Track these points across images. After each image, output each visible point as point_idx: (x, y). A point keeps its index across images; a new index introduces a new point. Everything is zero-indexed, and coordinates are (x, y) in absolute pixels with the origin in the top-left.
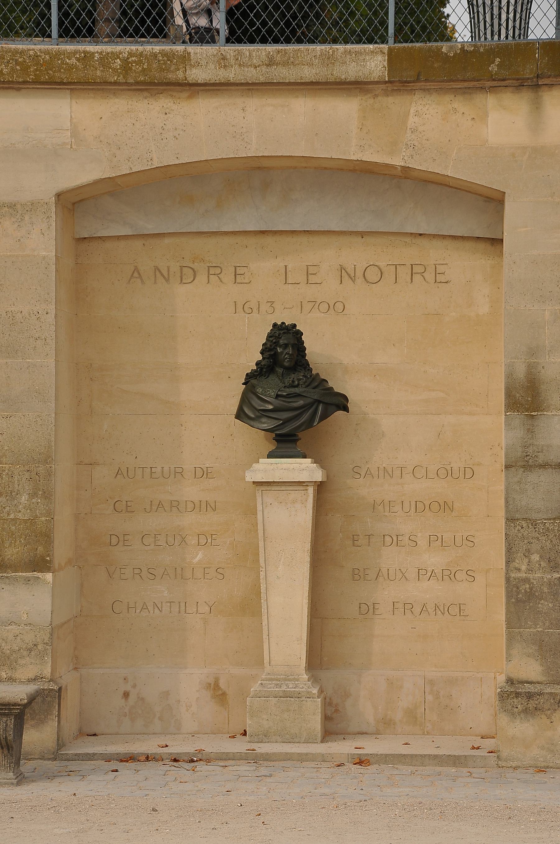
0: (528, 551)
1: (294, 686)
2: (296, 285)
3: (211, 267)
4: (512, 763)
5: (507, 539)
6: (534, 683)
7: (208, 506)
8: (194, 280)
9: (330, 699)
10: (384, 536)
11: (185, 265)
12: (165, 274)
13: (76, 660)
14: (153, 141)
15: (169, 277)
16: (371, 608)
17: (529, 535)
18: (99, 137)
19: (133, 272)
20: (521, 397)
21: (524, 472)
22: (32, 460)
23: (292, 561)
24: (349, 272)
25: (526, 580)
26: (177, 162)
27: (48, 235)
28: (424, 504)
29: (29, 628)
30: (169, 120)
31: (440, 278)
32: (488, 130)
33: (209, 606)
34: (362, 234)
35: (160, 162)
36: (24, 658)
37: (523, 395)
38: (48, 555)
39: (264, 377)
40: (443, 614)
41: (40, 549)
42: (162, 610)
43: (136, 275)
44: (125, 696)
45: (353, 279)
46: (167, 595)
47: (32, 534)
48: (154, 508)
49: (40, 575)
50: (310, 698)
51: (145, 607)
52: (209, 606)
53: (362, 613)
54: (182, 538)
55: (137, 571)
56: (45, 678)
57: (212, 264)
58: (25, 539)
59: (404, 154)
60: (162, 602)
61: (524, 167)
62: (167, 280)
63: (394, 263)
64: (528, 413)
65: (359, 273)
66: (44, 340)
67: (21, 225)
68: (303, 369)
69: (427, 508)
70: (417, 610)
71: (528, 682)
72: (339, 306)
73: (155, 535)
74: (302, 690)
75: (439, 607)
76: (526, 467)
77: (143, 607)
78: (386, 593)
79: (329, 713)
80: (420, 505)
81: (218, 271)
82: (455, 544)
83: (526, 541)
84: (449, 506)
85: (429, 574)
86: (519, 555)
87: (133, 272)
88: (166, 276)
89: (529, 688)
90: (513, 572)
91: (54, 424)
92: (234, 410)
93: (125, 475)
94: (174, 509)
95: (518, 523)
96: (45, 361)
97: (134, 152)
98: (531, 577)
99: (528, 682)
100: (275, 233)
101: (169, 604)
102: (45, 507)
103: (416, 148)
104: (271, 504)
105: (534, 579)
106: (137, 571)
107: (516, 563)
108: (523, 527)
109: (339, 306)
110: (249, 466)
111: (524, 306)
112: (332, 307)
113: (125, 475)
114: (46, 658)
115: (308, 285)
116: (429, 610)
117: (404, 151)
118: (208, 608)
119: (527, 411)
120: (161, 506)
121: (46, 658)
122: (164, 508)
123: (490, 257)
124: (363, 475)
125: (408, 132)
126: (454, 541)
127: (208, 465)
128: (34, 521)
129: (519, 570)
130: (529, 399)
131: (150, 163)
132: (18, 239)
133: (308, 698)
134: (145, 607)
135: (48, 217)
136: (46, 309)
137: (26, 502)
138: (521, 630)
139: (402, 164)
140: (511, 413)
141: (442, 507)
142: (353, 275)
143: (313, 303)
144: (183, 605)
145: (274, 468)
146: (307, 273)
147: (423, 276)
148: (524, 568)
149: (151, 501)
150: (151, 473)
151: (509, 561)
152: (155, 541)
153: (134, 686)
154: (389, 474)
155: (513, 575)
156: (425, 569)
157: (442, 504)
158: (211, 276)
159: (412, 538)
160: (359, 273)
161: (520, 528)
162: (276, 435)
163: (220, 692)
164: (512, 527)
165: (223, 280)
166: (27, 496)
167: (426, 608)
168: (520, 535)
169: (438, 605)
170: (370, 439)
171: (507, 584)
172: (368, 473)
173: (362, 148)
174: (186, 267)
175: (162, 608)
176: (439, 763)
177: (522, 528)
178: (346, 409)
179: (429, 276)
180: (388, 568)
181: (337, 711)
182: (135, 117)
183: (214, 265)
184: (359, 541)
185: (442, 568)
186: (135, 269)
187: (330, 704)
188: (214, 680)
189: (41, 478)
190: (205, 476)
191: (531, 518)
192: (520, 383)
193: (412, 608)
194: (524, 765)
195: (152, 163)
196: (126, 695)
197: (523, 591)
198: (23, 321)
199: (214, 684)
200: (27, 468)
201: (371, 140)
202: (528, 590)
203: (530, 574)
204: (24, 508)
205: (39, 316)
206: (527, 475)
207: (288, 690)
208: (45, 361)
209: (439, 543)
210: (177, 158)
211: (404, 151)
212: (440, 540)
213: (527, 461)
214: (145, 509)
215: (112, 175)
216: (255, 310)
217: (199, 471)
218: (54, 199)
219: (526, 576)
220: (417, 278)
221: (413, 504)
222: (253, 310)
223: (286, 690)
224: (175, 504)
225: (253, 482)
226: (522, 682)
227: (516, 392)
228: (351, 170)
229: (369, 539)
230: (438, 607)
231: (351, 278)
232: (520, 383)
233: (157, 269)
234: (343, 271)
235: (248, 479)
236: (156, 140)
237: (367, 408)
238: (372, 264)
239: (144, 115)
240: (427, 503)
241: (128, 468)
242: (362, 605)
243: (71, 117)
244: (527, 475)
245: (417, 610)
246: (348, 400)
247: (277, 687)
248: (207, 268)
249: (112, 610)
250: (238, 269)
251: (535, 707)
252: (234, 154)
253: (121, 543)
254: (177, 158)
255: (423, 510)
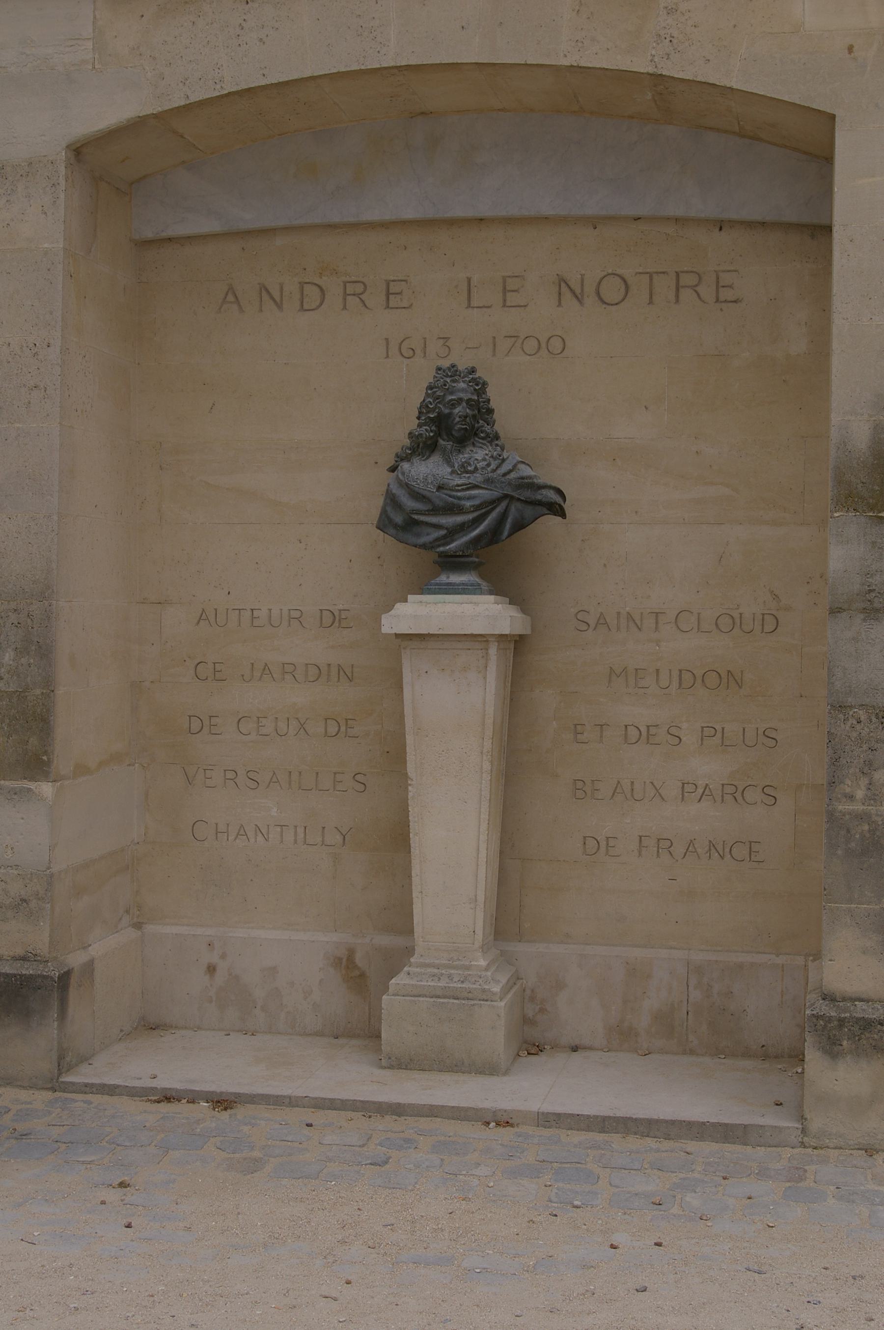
0: (869, 764)
1: (462, 979)
2: (485, 309)
3: (350, 282)
4: (828, 1141)
5: (830, 741)
6: (872, 1001)
7: (342, 672)
8: (321, 304)
9: (533, 991)
10: (626, 726)
11: (308, 281)
12: (276, 295)
13: (139, 910)
14: (224, 49)
15: (282, 303)
16: (603, 844)
17: (872, 734)
18: (138, 47)
19: (227, 294)
20: (862, 484)
21: (864, 620)
22: (21, 592)
23: (461, 770)
24: (572, 287)
25: (862, 817)
26: (263, 82)
27: (53, 214)
28: (693, 674)
29: (16, 872)
30: (252, 12)
31: (725, 294)
32: (804, 5)
33: (342, 834)
34: (594, 222)
35: (235, 83)
36: (8, 922)
37: (864, 481)
38: (45, 753)
39: (423, 457)
40: (722, 858)
41: (34, 741)
42: (268, 838)
43: (231, 298)
44: (209, 971)
45: (580, 300)
46: (275, 814)
47: (20, 717)
48: (257, 674)
49: (32, 785)
50: (487, 1000)
51: (242, 832)
52: (342, 834)
53: (587, 853)
54: (301, 724)
55: (230, 775)
56: (40, 956)
57: (350, 277)
58: (9, 725)
59: (653, 52)
60: (268, 826)
61: (869, 68)
62: (279, 306)
63: (648, 270)
64: (874, 513)
65: (590, 289)
66: (43, 391)
67: (12, 200)
68: (488, 444)
69: (699, 681)
70: (679, 849)
71: (861, 1000)
72: (556, 344)
73: (258, 718)
74: (474, 986)
75: (716, 846)
76: (868, 611)
77: (238, 833)
78: (629, 821)
79: (530, 1013)
80: (686, 676)
81: (359, 288)
82: (744, 741)
83: (865, 747)
84: (736, 678)
85: (700, 791)
86: (851, 771)
87: (227, 294)
88: (278, 299)
89: (864, 1010)
90: (840, 802)
91: (57, 533)
92: (375, 514)
93: (212, 620)
94: (288, 677)
95: (851, 713)
96: (43, 425)
97: (192, 69)
98: (872, 811)
99: (861, 1000)
100: (452, 223)
101: (279, 829)
102: (40, 671)
103: (675, 41)
104: (427, 672)
105: (877, 815)
106: (230, 775)
107: (846, 786)
108: (861, 721)
109: (556, 344)
110: (389, 608)
111: (869, 318)
112: (544, 345)
113: (212, 620)
114: (42, 924)
115: (506, 309)
116: (699, 850)
117: (654, 48)
118: (339, 838)
119: (872, 509)
120: (267, 672)
121: (42, 924)
122: (272, 675)
123: (809, 258)
124: (592, 625)
125: (661, 13)
126: (742, 737)
127: (341, 607)
128: (23, 695)
129: (851, 798)
130: (877, 488)
131: (218, 87)
132: (7, 223)
133: (483, 1000)
134: (242, 832)
135: (53, 184)
136: (47, 339)
137: (11, 663)
138: (852, 906)
139: (651, 70)
140: (842, 514)
141: (725, 680)
142: (578, 291)
143: (513, 339)
144: (300, 831)
145: (430, 611)
146: (505, 288)
147: (696, 291)
148: (860, 794)
149: (252, 664)
150: (253, 618)
151: (834, 782)
152: (258, 728)
153: (223, 956)
154: (636, 624)
155: (840, 807)
156: (694, 782)
157: (724, 675)
158: (349, 298)
159: (673, 731)
160: (590, 289)
161: (855, 722)
162: (441, 555)
163: (357, 973)
164: (840, 720)
165: (367, 303)
166: (12, 653)
167: (694, 847)
168: (855, 734)
169: (714, 843)
170: (605, 565)
171: (829, 823)
172: (602, 621)
173: (580, 44)
174: (309, 283)
175: (268, 833)
176: (698, 1135)
177: (858, 722)
178: (558, 510)
179: (707, 291)
180: (632, 780)
181: (542, 1010)
182: (196, 11)
183: (354, 279)
184: (585, 735)
185: (721, 782)
186: (229, 289)
187: (532, 999)
188: (347, 953)
189: (35, 623)
190: (336, 624)
191: (875, 704)
192: (859, 458)
193: (671, 847)
194: (850, 1146)
195: (223, 86)
196: (211, 969)
197: (857, 836)
198: (10, 359)
199: (348, 960)
200: (13, 605)
201: (595, 30)
202: (868, 835)
203: (872, 806)
204: (8, 673)
205: (36, 350)
206: (868, 626)
207: (452, 985)
208: (43, 425)
209: (717, 740)
210: (264, 75)
211: (654, 48)
212: (719, 735)
213: (869, 601)
214: (243, 676)
215: (156, 110)
216: (419, 352)
217: (327, 615)
218: (64, 154)
219: (863, 809)
220: (686, 294)
221: (675, 674)
222: (416, 351)
223: (447, 985)
224: (289, 668)
225: (396, 634)
226: (853, 1000)
227: (852, 475)
228: (574, 112)
229: (602, 731)
230: (713, 845)
231: (576, 297)
232: (859, 458)
233: (263, 288)
234: (563, 285)
235: (385, 630)
236: (230, 47)
237: (600, 514)
238: (610, 271)
239: (210, 7)
240: (699, 673)
241: (216, 610)
242: (589, 841)
243: (95, 17)
244: (868, 626)
245: (679, 849)
246: (564, 498)
247: (432, 980)
248: (342, 284)
249: (191, 834)
250: (392, 284)
251: (873, 1044)
252: (359, 63)
253: (206, 730)
254: (264, 75)
255: (691, 685)
